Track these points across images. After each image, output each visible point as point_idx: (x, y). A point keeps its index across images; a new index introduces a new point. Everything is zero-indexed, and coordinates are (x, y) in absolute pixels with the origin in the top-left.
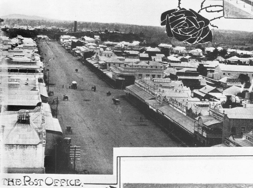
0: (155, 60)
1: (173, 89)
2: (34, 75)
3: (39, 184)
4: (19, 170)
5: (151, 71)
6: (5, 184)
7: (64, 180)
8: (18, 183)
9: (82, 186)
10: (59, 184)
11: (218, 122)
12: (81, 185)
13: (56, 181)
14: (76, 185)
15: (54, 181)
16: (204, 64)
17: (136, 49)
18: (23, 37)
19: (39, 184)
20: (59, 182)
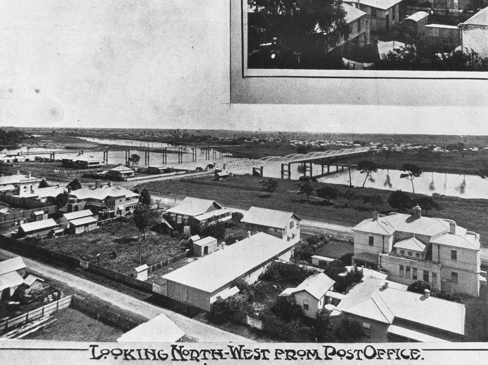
0: (382, 238)
1: (112, 42)
2: (355, 108)
3: (262, 356)
4: (183, 298)
5: (308, 167)
6: (177, 358)
7: (383, 350)
8: (248, 356)
9: (423, 359)
10: (394, 356)
11: (107, 171)
12: (420, 358)
13: (381, 352)
14: (413, 358)
15: (377, 351)
16: (366, 245)
17: (338, 153)
18: (385, 41)
19: (262, 356)
20: (386, 355)
